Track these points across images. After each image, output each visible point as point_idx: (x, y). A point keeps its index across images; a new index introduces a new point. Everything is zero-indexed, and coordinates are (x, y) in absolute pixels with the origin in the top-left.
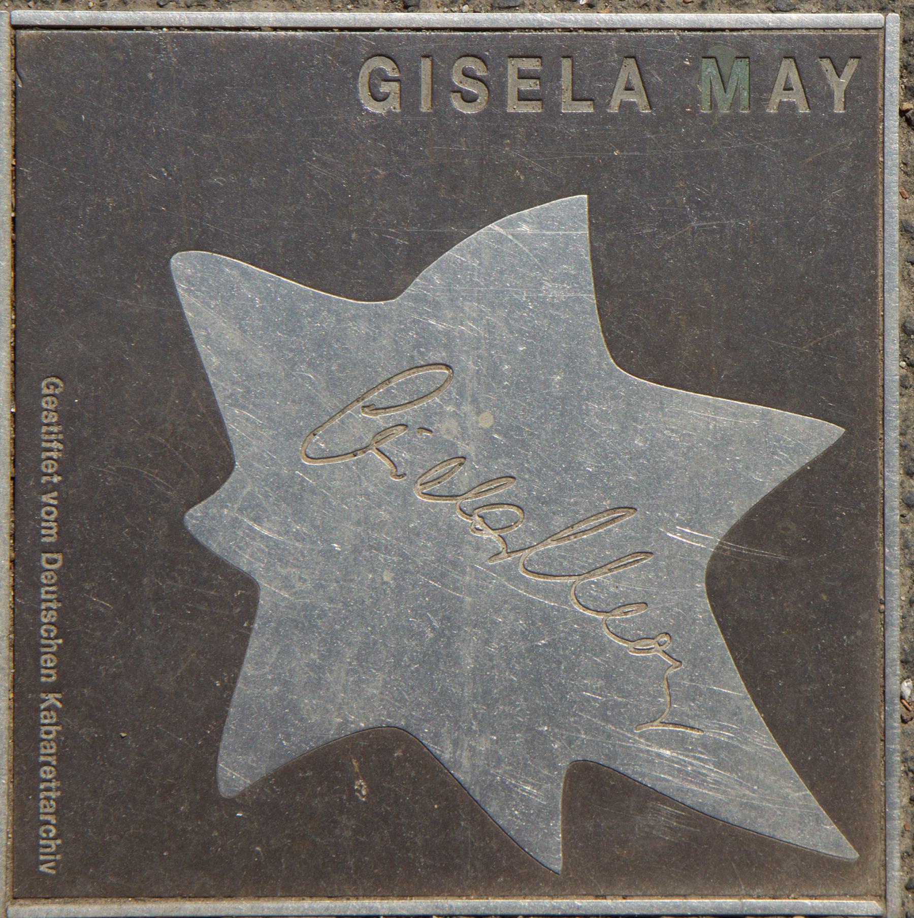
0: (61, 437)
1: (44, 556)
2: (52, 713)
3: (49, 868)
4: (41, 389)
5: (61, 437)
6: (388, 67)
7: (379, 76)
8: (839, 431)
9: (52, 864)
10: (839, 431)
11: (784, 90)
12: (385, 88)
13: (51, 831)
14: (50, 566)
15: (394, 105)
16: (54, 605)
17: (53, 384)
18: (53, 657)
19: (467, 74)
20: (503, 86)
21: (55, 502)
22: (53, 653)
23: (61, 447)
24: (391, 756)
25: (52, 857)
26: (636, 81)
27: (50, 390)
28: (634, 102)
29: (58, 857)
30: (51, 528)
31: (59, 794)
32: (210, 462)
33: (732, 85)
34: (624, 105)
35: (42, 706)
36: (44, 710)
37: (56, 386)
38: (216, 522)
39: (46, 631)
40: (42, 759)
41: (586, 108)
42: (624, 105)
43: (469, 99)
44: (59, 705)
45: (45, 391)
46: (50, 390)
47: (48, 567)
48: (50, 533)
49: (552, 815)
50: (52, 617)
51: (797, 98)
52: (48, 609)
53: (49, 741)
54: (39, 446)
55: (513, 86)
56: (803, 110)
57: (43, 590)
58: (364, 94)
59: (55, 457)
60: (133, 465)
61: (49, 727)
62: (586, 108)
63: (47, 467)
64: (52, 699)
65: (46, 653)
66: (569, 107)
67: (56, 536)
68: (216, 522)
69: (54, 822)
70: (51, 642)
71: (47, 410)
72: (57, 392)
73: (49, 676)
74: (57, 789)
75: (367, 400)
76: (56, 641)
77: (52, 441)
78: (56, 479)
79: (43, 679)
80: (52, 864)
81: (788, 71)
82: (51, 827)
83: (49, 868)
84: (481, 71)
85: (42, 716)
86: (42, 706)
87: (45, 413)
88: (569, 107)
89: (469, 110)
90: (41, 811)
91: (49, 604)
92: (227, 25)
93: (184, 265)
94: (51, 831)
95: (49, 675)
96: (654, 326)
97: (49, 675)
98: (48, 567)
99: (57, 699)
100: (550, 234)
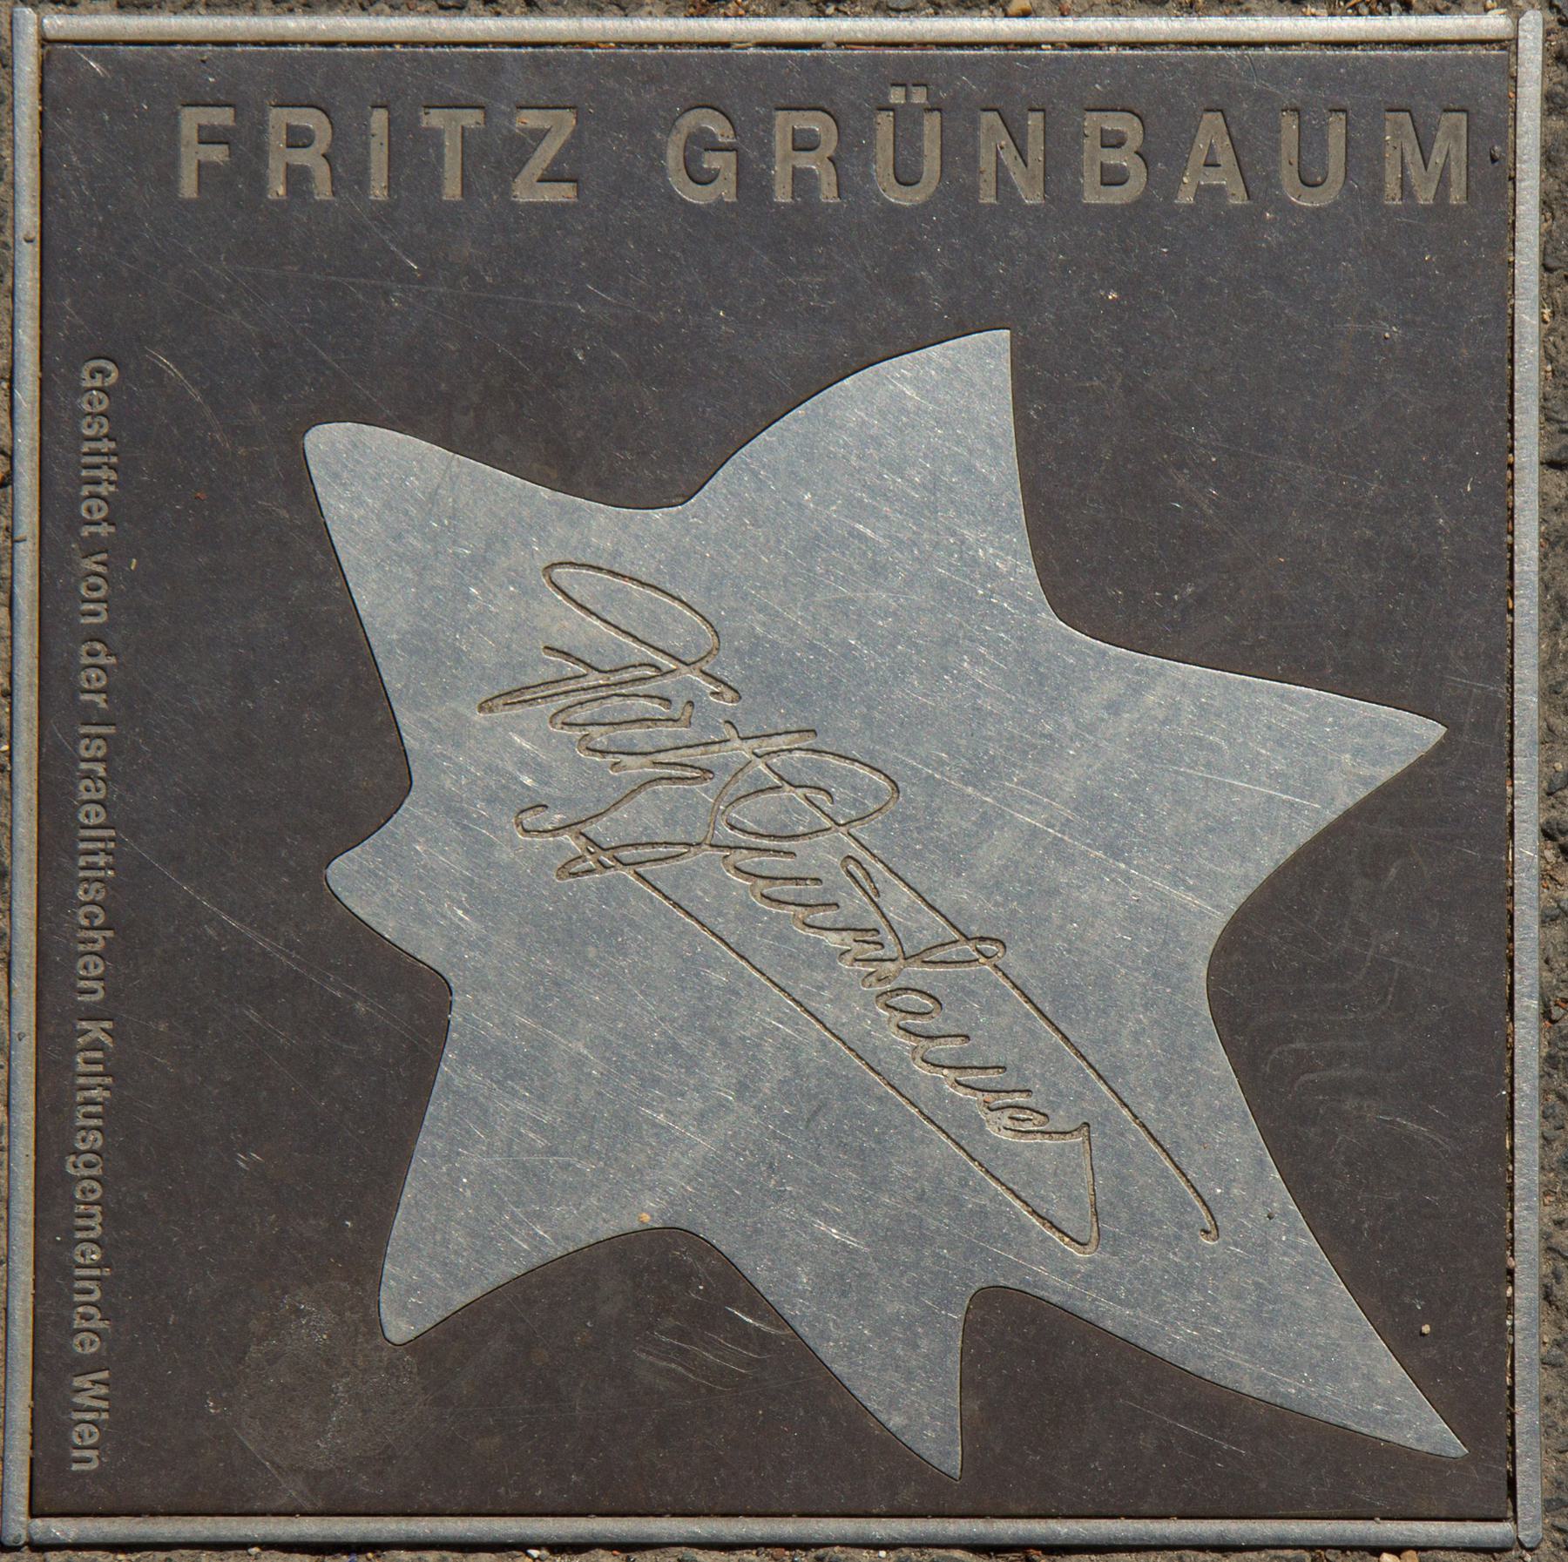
5: (114, 460)
6: (718, 127)
7: (702, 142)
8: (1431, 732)
10: (1431, 732)
11: (1206, 165)
12: (713, 161)
15: (725, 190)
17: (101, 371)
18: (99, 808)
20: (767, 153)
21: (100, 569)
22: (78, 1153)
23: (114, 477)
24: (670, 1282)
25: (97, 1272)
26: (1226, 157)
28: (1221, 187)
30: (91, 1216)
32: (362, 773)
33: (1437, 159)
34: (1201, 191)
37: (105, 373)
38: (363, 882)
42: (1201, 191)
44: (107, 1040)
45: (87, 384)
46: (97, 380)
49: (952, 1442)
50: (96, 892)
51: (1226, 178)
54: (73, 986)
58: (674, 156)
59: (105, 493)
61: (93, 1091)
63: (87, 816)
64: (96, 1030)
68: (363, 882)
70: (91, 934)
73: (95, 614)
75: (641, 870)
77: (98, 467)
78: (104, 530)
81: (1211, 132)
85: (81, 788)
87: (87, 741)
91: (91, 859)
93: (327, 443)
95: (86, 1345)
96: (1128, 544)
97: (86, 1345)
99: (103, 1030)
100: (945, 402)
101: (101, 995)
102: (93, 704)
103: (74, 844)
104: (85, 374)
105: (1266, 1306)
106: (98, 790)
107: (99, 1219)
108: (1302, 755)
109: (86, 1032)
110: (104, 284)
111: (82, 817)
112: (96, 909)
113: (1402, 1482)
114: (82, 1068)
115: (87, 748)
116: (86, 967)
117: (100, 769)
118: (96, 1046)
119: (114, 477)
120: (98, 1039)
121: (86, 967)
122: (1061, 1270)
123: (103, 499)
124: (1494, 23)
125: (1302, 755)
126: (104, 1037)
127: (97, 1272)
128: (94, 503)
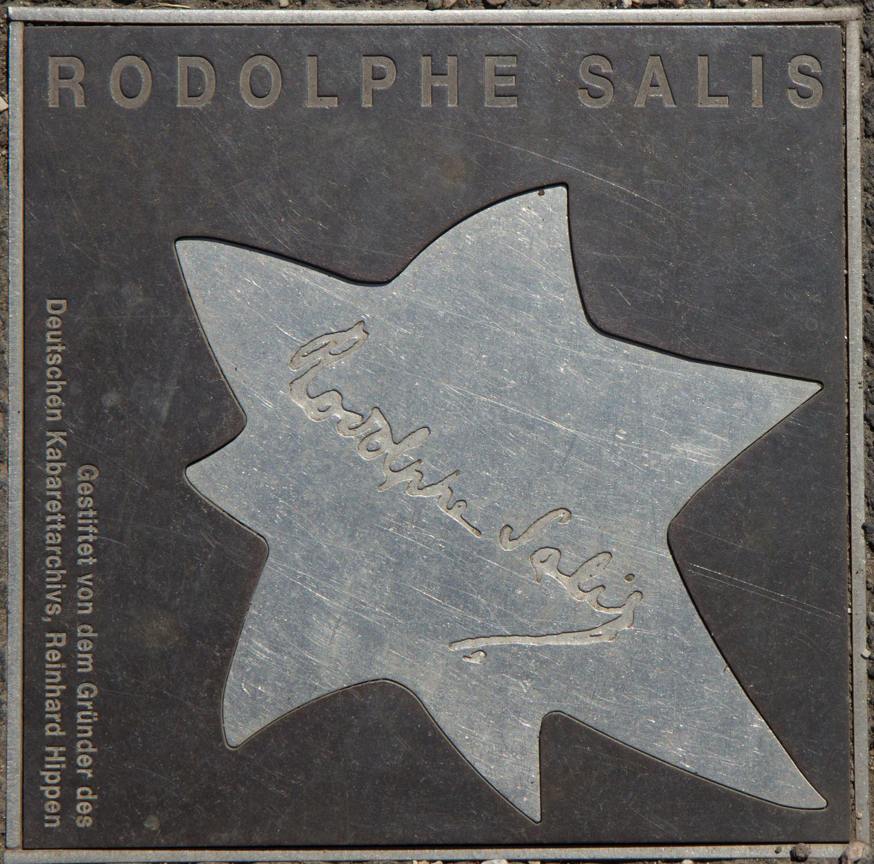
0: (96, 521)
1: (50, 302)
2: (58, 451)
3: (55, 596)
4: (76, 694)
5: (96, 521)
9: (59, 592)
10: (815, 387)
13: (56, 561)
14: (85, 693)
16: (59, 348)
17: (88, 689)
19: (803, 71)
21: (59, 600)
25: (58, 666)
26: (661, 78)
27: (55, 308)
29: (64, 666)
30: (87, 660)
31: (96, 538)
32: (213, 417)
34: (650, 102)
35: (49, 444)
36: (50, 447)
38: (217, 480)
39: (51, 373)
40: (48, 716)
41: (722, 103)
42: (650, 102)
43: (804, 95)
44: (64, 443)
45: (57, 789)
46: (87, 479)
47: (54, 312)
48: (86, 664)
50: (58, 359)
52: (55, 352)
53: (53, 476)
55: (489, 82)
56: (669, 105)
57: (48, 334)
59: (59, 350)
60: (137, 396)
62: (722, 103)
64: (57, 437)
65: (57, 330)
66: (312, 102)
67: (91, 666)
68: (217, 480)
69: (59, 720)
71: (82, 496)
72: (94, 478)
73: (53, 415)
74: (62, 522)
76: (61, 464)
77: (87, 525)
79: (49, 419)
80: (59, 592)
81: (653, 67)
82: (57, 558)
83: (55, 596)
84: (816, 69)
85: (47, 538)
86: (49, 444)
87: (82, 498)
88: (312, 102)
89: (801, 105)
90: (47, 709)
91: (54, 348)
92: (468, 22)
94: (56, 561)
96: (638, 293)
98: (54, 312)
101: (58, 823)
102: (86, 775)
103: (63, 333)
104: (79, 691)
105: (710, 728)
106: (56, 706)
107: (91, 661)
108: (717, 415)
109: (53, 438)
110: (60, 158)
111: (80, 552)
112: (56, 369)
113: (791, 828)
114: (80, 720)
115: (51, 360)
116: (51, 656)
117: (58, 494)
118: (56, 446)
119: (96, 531)
120: (58, 442)
121: (50, 807)
122: (595, 710)
123: (59, 353)
124: (16, 31)
125: (717, 415)
126: (61, 440)
127: (58, 666)
128: (86, 546)
